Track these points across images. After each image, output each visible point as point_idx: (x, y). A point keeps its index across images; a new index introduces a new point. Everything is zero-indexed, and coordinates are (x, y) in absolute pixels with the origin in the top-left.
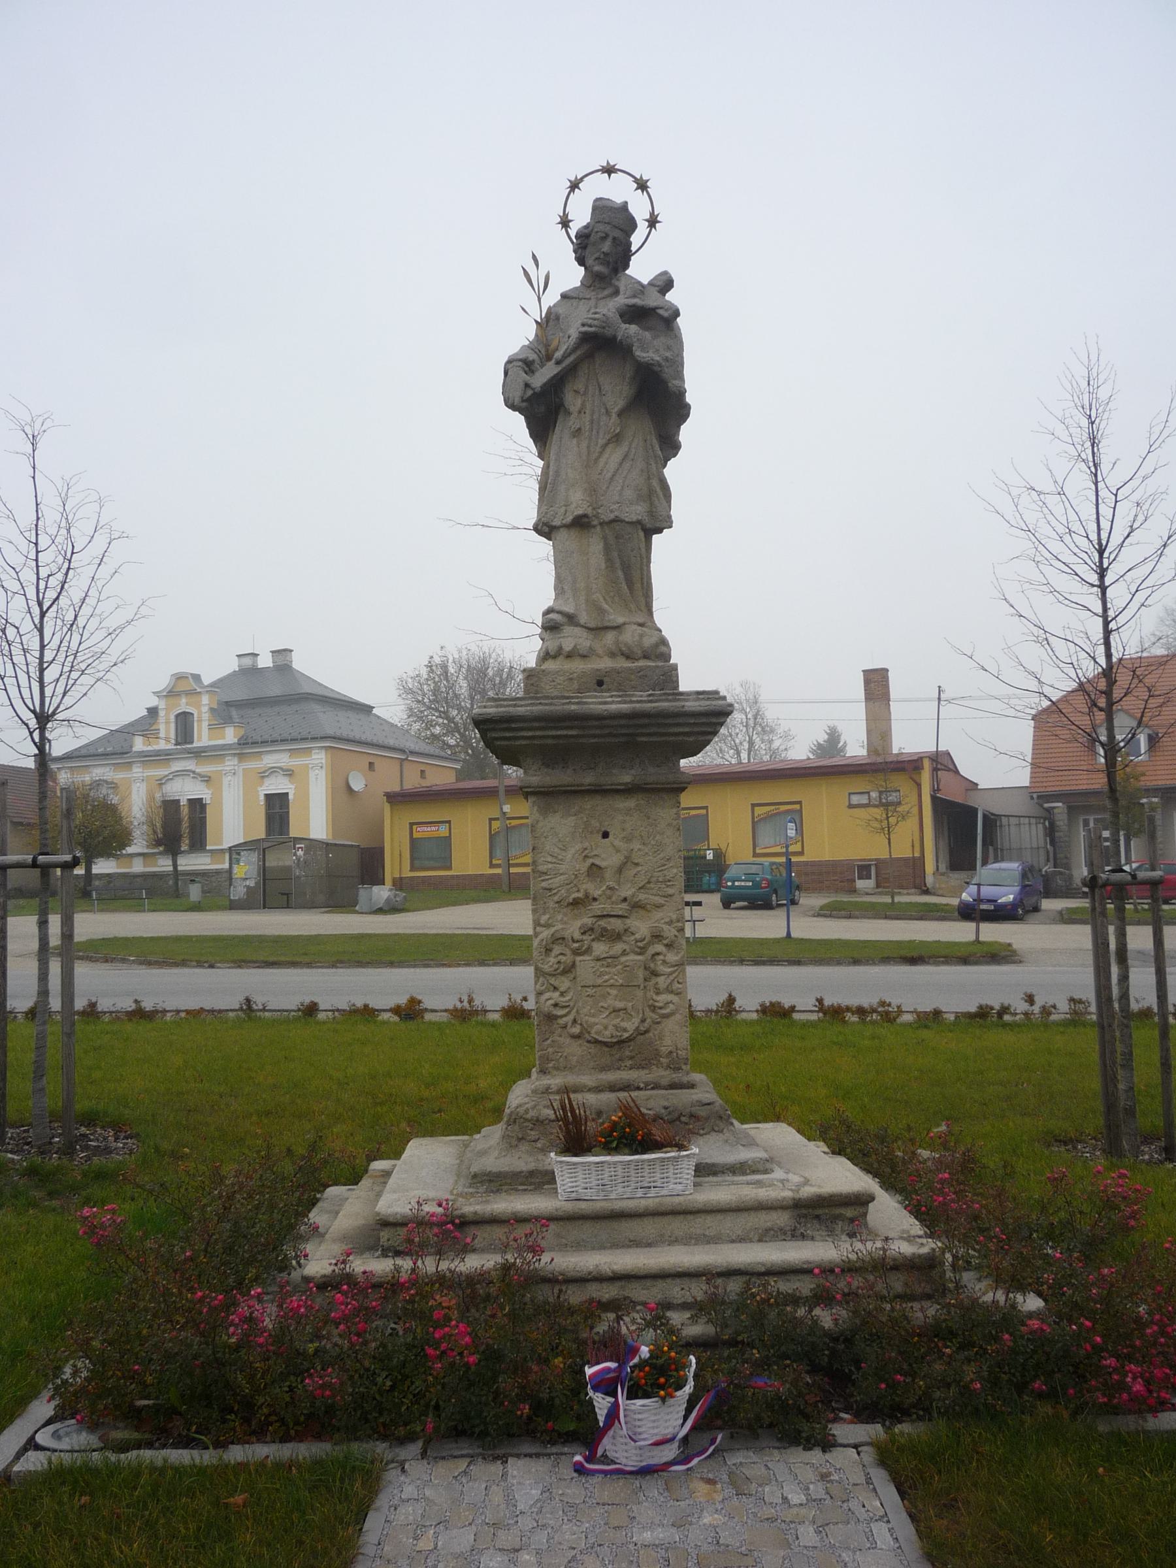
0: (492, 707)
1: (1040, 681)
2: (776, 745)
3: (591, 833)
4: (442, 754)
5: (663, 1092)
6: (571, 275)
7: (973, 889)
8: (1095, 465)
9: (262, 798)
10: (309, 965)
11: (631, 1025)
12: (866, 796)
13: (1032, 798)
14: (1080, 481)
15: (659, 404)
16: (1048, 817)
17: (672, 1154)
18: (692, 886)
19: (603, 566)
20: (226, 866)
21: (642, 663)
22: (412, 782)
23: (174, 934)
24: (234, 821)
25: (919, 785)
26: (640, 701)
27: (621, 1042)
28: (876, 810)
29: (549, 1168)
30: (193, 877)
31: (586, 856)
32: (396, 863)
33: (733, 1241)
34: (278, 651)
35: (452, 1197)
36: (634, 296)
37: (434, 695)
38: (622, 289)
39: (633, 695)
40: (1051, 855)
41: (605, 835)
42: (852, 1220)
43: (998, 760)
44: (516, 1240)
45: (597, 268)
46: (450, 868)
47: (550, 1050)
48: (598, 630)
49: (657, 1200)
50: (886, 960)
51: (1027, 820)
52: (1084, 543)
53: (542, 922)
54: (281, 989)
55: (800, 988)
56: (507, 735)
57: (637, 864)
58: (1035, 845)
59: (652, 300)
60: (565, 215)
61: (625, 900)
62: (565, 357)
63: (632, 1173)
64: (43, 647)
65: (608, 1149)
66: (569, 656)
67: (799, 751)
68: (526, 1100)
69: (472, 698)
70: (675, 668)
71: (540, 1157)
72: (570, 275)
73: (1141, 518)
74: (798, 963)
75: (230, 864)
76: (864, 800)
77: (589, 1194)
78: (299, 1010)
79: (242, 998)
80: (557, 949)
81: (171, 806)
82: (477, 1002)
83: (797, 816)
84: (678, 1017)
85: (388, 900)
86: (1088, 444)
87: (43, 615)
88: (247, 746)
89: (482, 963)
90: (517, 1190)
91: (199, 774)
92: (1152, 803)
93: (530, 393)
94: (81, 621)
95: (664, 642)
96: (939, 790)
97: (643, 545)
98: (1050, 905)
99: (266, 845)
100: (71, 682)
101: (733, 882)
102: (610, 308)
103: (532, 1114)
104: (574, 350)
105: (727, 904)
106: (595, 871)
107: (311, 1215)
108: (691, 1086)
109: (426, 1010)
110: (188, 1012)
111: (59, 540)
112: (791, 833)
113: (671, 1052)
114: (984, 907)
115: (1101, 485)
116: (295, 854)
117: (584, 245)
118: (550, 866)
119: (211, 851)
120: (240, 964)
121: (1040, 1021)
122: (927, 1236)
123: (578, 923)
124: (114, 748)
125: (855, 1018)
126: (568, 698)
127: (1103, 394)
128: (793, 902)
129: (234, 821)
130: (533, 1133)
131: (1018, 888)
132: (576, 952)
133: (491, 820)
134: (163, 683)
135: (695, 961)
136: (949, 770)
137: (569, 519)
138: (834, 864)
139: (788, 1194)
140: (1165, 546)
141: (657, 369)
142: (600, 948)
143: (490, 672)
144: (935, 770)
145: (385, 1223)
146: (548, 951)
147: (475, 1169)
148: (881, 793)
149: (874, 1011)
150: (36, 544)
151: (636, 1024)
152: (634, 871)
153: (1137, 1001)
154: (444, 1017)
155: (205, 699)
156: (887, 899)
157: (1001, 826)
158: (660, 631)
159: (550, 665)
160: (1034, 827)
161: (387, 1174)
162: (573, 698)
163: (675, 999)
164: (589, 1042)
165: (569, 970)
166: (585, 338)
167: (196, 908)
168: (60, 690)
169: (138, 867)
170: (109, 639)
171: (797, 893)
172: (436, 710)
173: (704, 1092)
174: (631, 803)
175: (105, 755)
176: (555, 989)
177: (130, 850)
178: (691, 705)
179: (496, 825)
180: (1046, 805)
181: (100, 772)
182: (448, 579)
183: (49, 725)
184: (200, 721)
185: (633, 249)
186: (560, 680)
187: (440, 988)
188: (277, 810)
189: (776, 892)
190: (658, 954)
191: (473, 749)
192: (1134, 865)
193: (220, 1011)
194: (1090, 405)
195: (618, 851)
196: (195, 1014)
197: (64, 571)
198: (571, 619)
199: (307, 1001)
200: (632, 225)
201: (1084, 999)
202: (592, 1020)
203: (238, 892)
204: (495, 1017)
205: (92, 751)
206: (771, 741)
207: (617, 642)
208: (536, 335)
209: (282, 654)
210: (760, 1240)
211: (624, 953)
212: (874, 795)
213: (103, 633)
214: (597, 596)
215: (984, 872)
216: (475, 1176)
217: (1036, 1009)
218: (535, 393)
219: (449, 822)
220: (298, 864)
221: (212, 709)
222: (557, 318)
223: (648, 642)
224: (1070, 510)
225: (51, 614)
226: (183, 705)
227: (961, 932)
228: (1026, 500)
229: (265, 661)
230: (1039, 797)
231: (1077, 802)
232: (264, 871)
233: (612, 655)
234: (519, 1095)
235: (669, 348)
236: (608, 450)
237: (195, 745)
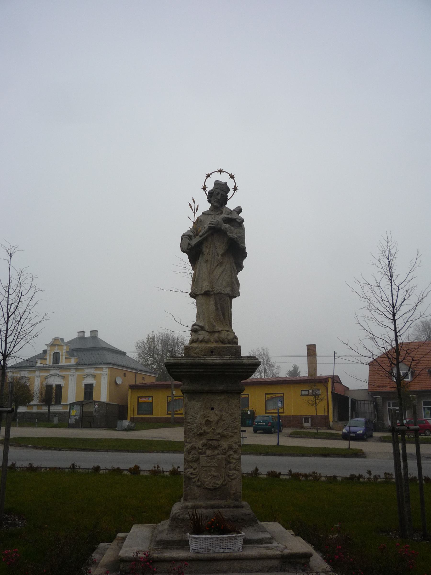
0: (172, 360)
1: (372, 354)
2: (274, 371)
3: (207, 408)
4: (151, 371)
5: (231, 509)
6: (206, 206)
7: (347, 428)
8: (391, 277)
9: (83, 385)
10: (97, 451)
11: (220, 482)
12: (308, 392)
13: (369, 394)
14: (385, 282)
15: (236, 252)
16: (375, 401)
17: (234, 535)
18: (244, 425)
19: (214, 309)
20: (68, 410)
21: (228, 345)
22: (140, 381)
23: (47, 436)
24: (72, 394)
25: (327, 388)
26: (227, 359)
27: (216, 489)
28: (311, 397)
29: (187, 539)
30: (56, 414)
31: (205, 417)
32: (132, 411)
33: (257, 572)
34: (93, 331)
35: (148, 550)
36: (228, 214)
37: (149, 349)
38: (224, 211)
39: (224, 357)
40: (376, 415)
41: (212, 409)
42: (304, 564)
43: (356, 378)
44: (174, 570)
45: (215, 204)
46: (152, 414)
47: (189, 491)
48: (212, 333)
49: (228, 554)
50: (315, 455)
51: (367, 402)
52: (387, 304)
53: (188, 441)
54: (87, 460)
55: (283, 465)
56: (177, 370)
57: (224, 420)
58: (370, 411)
59: (234, 216)
60: (205, 186)
61: (219, 434)
62: (203, 234)
63: (219, 543)
64: (7, 330)
65: (210, 533)
66: (201, 342)
67: (283, 374)
68: (179, 511)
69: (163, 351)
70: (239, 347)
71: (184, 534)
72: (205, 206)
73: (407, 296)
74: (281, 455)
75: (70, 410)
76: (306, 393)
77: (202, 551)
78: (93, 469)
79: (71, 464)
80: (193, 452)
81: (49, 387)
82: (161, 468)
83: (282, 399)
84: (238, 479)
85: (128, 426)
86: (388, 269)
87: (8, 318)
88: (79, 366)
89: (163, 452)
90: (174, 548)
91: (61, 376)
92: (413, 397)
93: (190, 247)
94: (22, 321)
95: (236, 337)
96: (334, 390)
97: (229, 303)
98: (376, 435)
99: (84, 403)
100: (17, 343)
101: (258, 423)
102: (219, 218)
103: (181, 517)
104: (206, 232)
105: (255, 431)
106: (208, 422)
107: (93, 555)
108: (242, 507)
109: (141, 470)
110: (50, 468)
111: (17, 291)
112: (280, 405)
113: (235, 493)
114: (352, 435)
115: (393, 283)
116: (94, 407)
117: (211, 196)
118: (191, 420)
119: (63, 405)
120: (71, 449)
121: (373, 481)
122: (333, 571)
123: (201, 442)
124: (30, 364)
125: (303, 479)
126: (200, 357)
127: (393, 251)
128: (280, 431)
129: (72, 394)
130: (181, 525)
131: (364, 428)
132: (200, 453)
133: (168, 397)
134: (49, 341)
135: (244, 453)
136: (339, 383)
137: (203, 292)
138: (295, 417)
139: (279, 553)
140: (417, 305)
141: (236, 240)
142: (209, 452)
143: (170, 341)
144: (333, 382)
145: (122, 560)
146: (189, 452)
147: (158, 539)
148: (313, 390)
149: (310, 475)
150: (8, 292)
151: (222, 482)
152: (222, 423)
153: (410, 475)
154: (148, 474)
155: (65, 348)
156: (315, 431)
157: (357, 404)
158: (235, 333)
159: (194, 345)
160: (370, 405)
161: (124, 539)
162: (202, 357)
163: (237, 472)
164: (203, 488)
165: (197, 460)
166: (210, 228)
167: (56, 426)
168: (13, 345)
169: (35, 410)
170: (32, 328)
171: (281, 428)
172: (150, 355)
173: (247, 510)
174: (222, 397)
175: (26, 367)
176: (192, 467)
177: (31, 403)
178: (245, 361)
179: (170, 398)
180: (374, 397)
181: (24, 373)
182: (157, 307)
183: (7, 359)
184: (62, 356)
185: (228, 198)
186: (197, 350)
187: (147, 461)
188: (89, 390)
189: (273, 427)
190: (231, 455)
191: (162, 369)
192: (407, 420)
193: (62, 468)
194: (389, 255)
195: (217, 415)
196: (53, 469)
197: (17, 302)
198: (202, 328)
199: (96, 466)
200: (228, 190)
201: (390, 473)
202: (206, 480)
203: (72, 421)
204: (167, 474)
205: (21, 365)
206: (272, 370)
207: (219, 337)
208: (193, 227)
209: (94, 333)
210: (268, 572)
211: (218, 454)
212: (310, 391)
213: (30, 325)
214: (212, 320)
215: (352, 421)
216: (158, 542)
217: (372, 476)
218: (192, 247)
219: (152, 397)
220: (95, 411)
221: (67, 352)
222: (201, 221)
223: (230, 337)
224: (382, 292)
225: (12, 317)
226: (56, 350)
227: (343, 445)
228: (366, 288)
229: (88, 335)
230: (371, 393)
231: (386, 396)
232: (82, 413)
233: (217, 342)
234: (176, 509)
235: (240, 233)
236: (218, 268)
237: (60, 364)
